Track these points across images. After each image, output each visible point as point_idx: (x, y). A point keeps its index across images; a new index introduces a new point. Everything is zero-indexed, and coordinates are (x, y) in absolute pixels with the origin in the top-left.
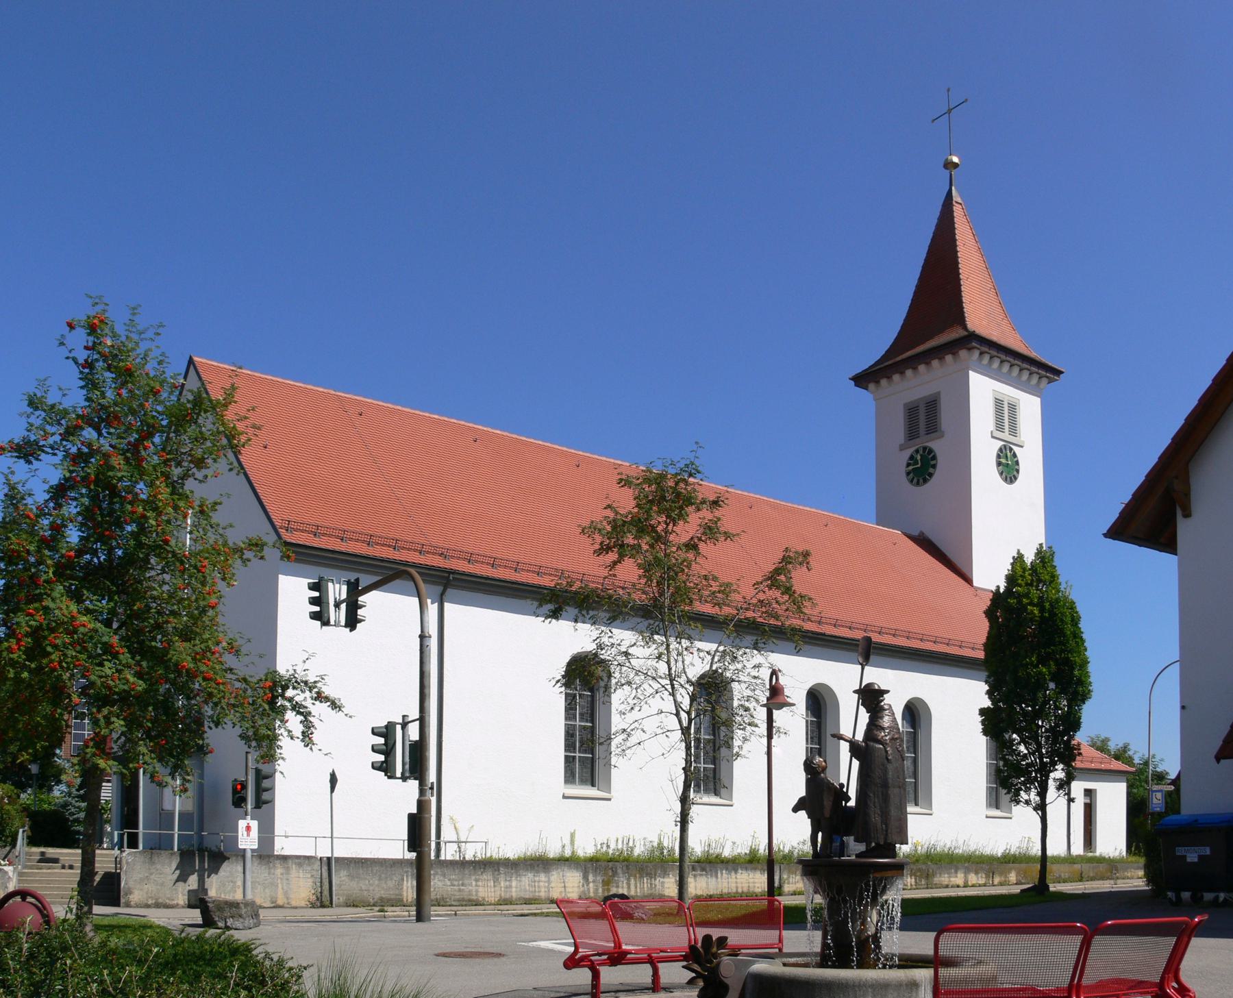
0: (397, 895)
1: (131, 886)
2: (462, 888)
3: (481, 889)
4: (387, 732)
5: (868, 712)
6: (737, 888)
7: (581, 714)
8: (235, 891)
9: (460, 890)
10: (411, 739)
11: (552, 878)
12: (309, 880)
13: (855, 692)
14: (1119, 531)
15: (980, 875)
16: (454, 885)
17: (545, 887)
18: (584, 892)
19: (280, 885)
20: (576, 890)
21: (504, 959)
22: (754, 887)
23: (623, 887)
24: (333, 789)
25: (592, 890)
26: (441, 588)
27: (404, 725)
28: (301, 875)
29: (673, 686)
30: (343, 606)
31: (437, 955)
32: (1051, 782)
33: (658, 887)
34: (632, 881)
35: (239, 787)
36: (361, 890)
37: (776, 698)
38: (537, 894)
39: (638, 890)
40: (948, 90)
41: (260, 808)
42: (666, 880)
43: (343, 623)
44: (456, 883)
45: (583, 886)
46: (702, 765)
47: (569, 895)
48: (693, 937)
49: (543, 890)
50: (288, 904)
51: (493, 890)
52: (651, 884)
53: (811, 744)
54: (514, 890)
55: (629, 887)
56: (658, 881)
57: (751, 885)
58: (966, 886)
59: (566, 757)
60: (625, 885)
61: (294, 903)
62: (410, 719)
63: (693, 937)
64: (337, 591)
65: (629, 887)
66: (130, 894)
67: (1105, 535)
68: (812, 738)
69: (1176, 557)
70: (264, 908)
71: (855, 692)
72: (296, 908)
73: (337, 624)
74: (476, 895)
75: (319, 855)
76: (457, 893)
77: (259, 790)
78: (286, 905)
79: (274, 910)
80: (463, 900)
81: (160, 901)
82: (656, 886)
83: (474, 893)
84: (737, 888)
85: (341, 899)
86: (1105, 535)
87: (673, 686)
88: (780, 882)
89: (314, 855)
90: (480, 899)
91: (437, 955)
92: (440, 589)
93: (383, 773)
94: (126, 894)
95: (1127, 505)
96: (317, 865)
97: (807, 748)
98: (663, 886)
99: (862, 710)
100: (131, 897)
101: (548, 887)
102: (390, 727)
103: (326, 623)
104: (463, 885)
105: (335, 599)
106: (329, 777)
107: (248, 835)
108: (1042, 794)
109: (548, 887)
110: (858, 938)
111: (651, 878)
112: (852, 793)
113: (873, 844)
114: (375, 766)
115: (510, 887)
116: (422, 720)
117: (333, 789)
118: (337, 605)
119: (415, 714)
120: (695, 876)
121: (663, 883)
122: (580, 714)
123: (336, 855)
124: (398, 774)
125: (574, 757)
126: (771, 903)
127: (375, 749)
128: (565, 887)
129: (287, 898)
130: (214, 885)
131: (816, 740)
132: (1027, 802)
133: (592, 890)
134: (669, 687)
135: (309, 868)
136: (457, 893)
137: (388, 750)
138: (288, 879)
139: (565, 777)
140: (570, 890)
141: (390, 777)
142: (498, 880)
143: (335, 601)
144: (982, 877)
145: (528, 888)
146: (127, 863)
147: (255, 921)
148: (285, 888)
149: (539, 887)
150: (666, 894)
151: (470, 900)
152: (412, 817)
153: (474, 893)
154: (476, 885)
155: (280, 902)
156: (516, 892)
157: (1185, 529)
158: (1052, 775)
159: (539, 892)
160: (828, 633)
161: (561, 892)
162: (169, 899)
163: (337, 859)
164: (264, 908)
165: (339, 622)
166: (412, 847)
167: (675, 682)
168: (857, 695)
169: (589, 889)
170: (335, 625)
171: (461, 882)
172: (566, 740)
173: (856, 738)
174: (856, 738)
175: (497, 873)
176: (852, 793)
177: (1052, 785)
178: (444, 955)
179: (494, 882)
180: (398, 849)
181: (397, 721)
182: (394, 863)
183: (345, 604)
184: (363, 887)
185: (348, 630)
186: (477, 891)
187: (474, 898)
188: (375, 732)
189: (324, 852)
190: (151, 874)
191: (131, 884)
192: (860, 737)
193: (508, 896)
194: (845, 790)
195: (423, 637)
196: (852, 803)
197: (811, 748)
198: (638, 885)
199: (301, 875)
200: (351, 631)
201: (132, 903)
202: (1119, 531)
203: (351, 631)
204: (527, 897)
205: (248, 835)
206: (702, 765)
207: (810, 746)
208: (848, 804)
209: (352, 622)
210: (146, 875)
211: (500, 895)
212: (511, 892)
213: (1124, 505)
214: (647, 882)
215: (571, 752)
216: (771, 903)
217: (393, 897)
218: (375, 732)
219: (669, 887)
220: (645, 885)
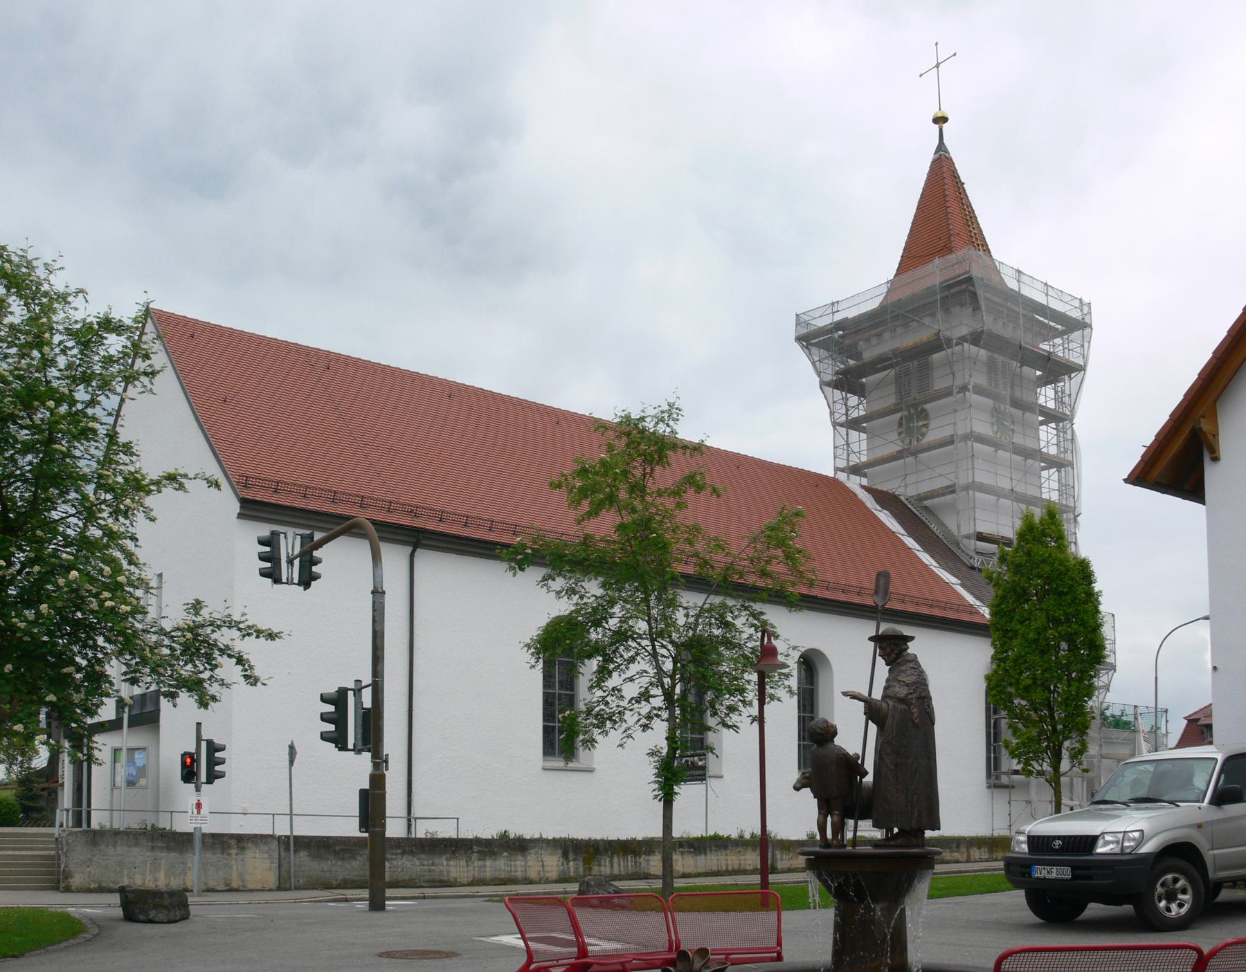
0: (362, 876)
1: (72, 869)
2: (433, 868)
3: (452, 869)
4: (338, 699)
5: (887, 665)
6: (727, 865)
7: (560, 682)
8: (186, 873)
9: (430, 871)
10: (364, 706)
11: (529, 858)
12: (266, 861)
13: (871, 639)
14: (1142, 476)
15: (983, 849)
16: (424, 865)
17: (521, 866)
18: (563, 872)
19: (234, 866)
20: (555, 869)
21: (456, 960)
22: (746, 864)
23: (605, 866)
24: (291, 762)
25: (572, 869)
26: (409, 549)
27: (358, 691)
28: (258, 856)
29: (654, 646)
30: (297, 562)
31: (381, 955)
32: (1064, 751)
33: (643, 865)
34: (616, 860)
35: (188, 760)
36: (323, 871)
37: (767, 655)
38: (513, 874)
39: (622, 869)
40: (937, 44)
41: (211, 783)
42: (651, 858)
43: (296, 581)
44: (426, 863)
45: (563, 865)
46: (689, 736)
47: (547, 875)
48: (674, 938)
49: (519, 869)
50: (243, 886)
51: (465, 870)
52: (636, 862)
53: (803, 713)
54: (488, 869)
55: (612, 866)
56: (642, 859)
57: (742, 862)
58: (968, 861)
59: (545, 727)
60: (607, 863)
61: (250, 886)
62: (363, 685)
63: (674, 938)
64: (290, 544)
65: (612, 866)
66: (71, 877)
67: (1126, 481)
68: (804, 706)
69: (1204, 507)
70: (217, 891)
71: (871, 639)
72: (252, 891)
73: (290, 582)
74: (448, 875)
75: (278, 833)
76: (427, 874)
77: (212, 762)
78: (241, 888)
79: (227, 894)
80: (434, 881)
81: (104, 884)
82: (640, 864)
83: (445, 874)
84: (727, 865)
85: (301, 880)
86: (1126, 481)
87: (654, 646)
88: (773, 860)
89: (271, 833)
90: (452, 880)
91: (381, 955)
92: (409, 549)
93: (334, 745)
94: (66, 878)
95: (1149, 448)
96: (275, 845)
97: (799, 716)
98: (648, 864)
99: (880, 662)
100: (72, 881)
101: (525, 866)
102: (343, 692)
103: (277, 580)
104: (433, 864)
105: (288, 553)
106: (287, 750)
107: (199, 812)
108: (1056, 766)
109: (525, 866)
110: (686, 729)
111: (635, 856)
112: (869, 765)
113: (896, 830)
114: (325, 737)
115: (485, 866)
116: (377, 688)
117: (291, 762)
118: (290, 562)
119: (367, 679)
120: (682, 853)
121: (648, 861)
122: (559, 682)
123: (294, 834)
124: (350, 746)
125: (553, 728)
126: (765, 883)
127: (324, 718)
128: (543, 866)
129: (243, 881)
130: (163, 867)
131: (808, 708)
132: (1041, 773)
133: (572, 869)
134: (649, 648)
135: (267, 848)
136: (427, 874)
137: (338, 719)
138: (243, 860)
139: (544, 748)
140: (549, 869)
141: (340, 749)
142: (471, 859)
143: (288, 557)
144: (985, 852)
145: (503, 868)
146: (67, 843)
147: (183, 912)
148: (240, 869)
149: (515, 866)
150: (652, 873)
151: (441, 881)
152: (363, 794)
153: (445, 874)
154: (448, 865)
155: (234, 885)
156: (491, 871)
157: (1213, 476)
158: (1067, 744)
159: (516, 871)
160: (820, 595)
161: (539, 872)
162: (113, 882)
163: (296, 838)
164: (217, 891)
165: (292, 579)
166: (365, 823)
167: (656, 643)
168: (873, 643)
169: (569, 868)
170: (287, 583)
171: (430, 862)
172: (545, 709)
173: (873, 696)
174: (873, 696)
175: (469, 852)
176: (869, 765)
177: (1065, 755)
178: (389, 955)
179: (467, 861)
180: (350, 828)
181: (349, 687)
182: (924, 698)
183: (298, 559)
184: (326, 868)
185: (302, 588)
186: (448, 872)
187: (445, 878)
188: (324, 699)
189: (282, 830)
190: (94, 856)
191: (72, 867)
192: (877, 695)
193: (482, 875)
194: (860, 762)
195: (378, 593)
196: (869, 779)
197: (804, 717)
198: (622, 863)
199: (258, 856)
200: (305, 589)
201: (73, 888)
202: (1142, 476)
203: (305, 589)
204: (503, 877)
205: (199, 812)
206: (689, 736)
207: (802, 714)
208: (864, 780)
209: (307, 579)
210: (89, 856)
211: (474, 875)
212: (485, 872)
213: (1145, 449)
214: (632, 861)
215: (550, 722)
216: (765, 883)
217: (357, 878)
218: (324, 699)
219: (654, 864)
220: (629, 863)
